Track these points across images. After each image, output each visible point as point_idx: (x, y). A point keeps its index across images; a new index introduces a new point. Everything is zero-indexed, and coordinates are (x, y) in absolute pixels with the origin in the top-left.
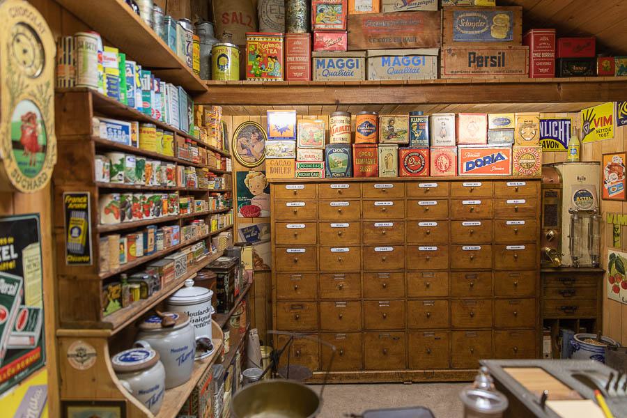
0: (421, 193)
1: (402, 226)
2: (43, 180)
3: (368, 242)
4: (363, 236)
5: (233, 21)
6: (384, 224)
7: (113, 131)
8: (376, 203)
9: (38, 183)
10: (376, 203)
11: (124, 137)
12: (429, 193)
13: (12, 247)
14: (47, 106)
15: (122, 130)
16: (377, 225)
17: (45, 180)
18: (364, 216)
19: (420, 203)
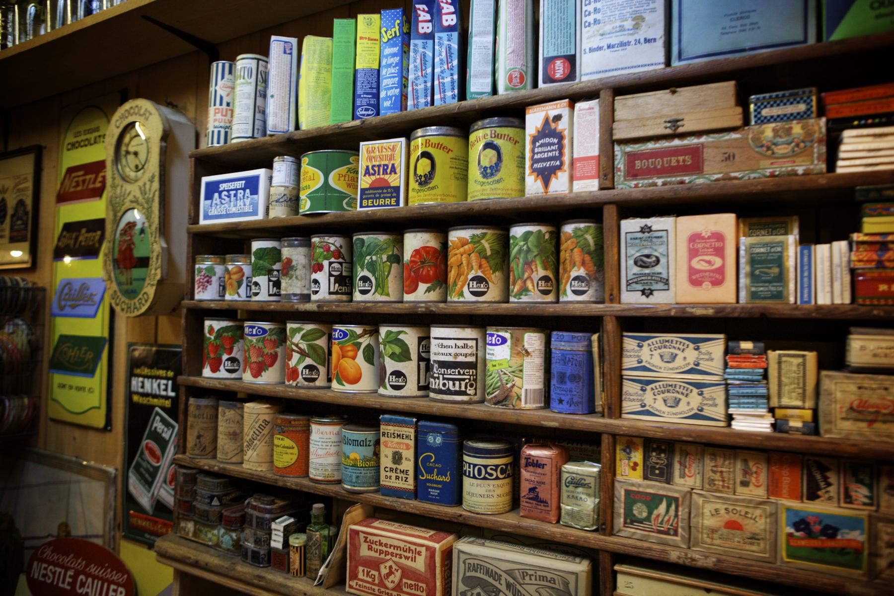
2: (143, 302)
7: (229, 196)
9: (138, 306)
11: (248, 201)
13: (170, 382)
14: (151, 207)
15: (244, 189)
17: (146, 301)
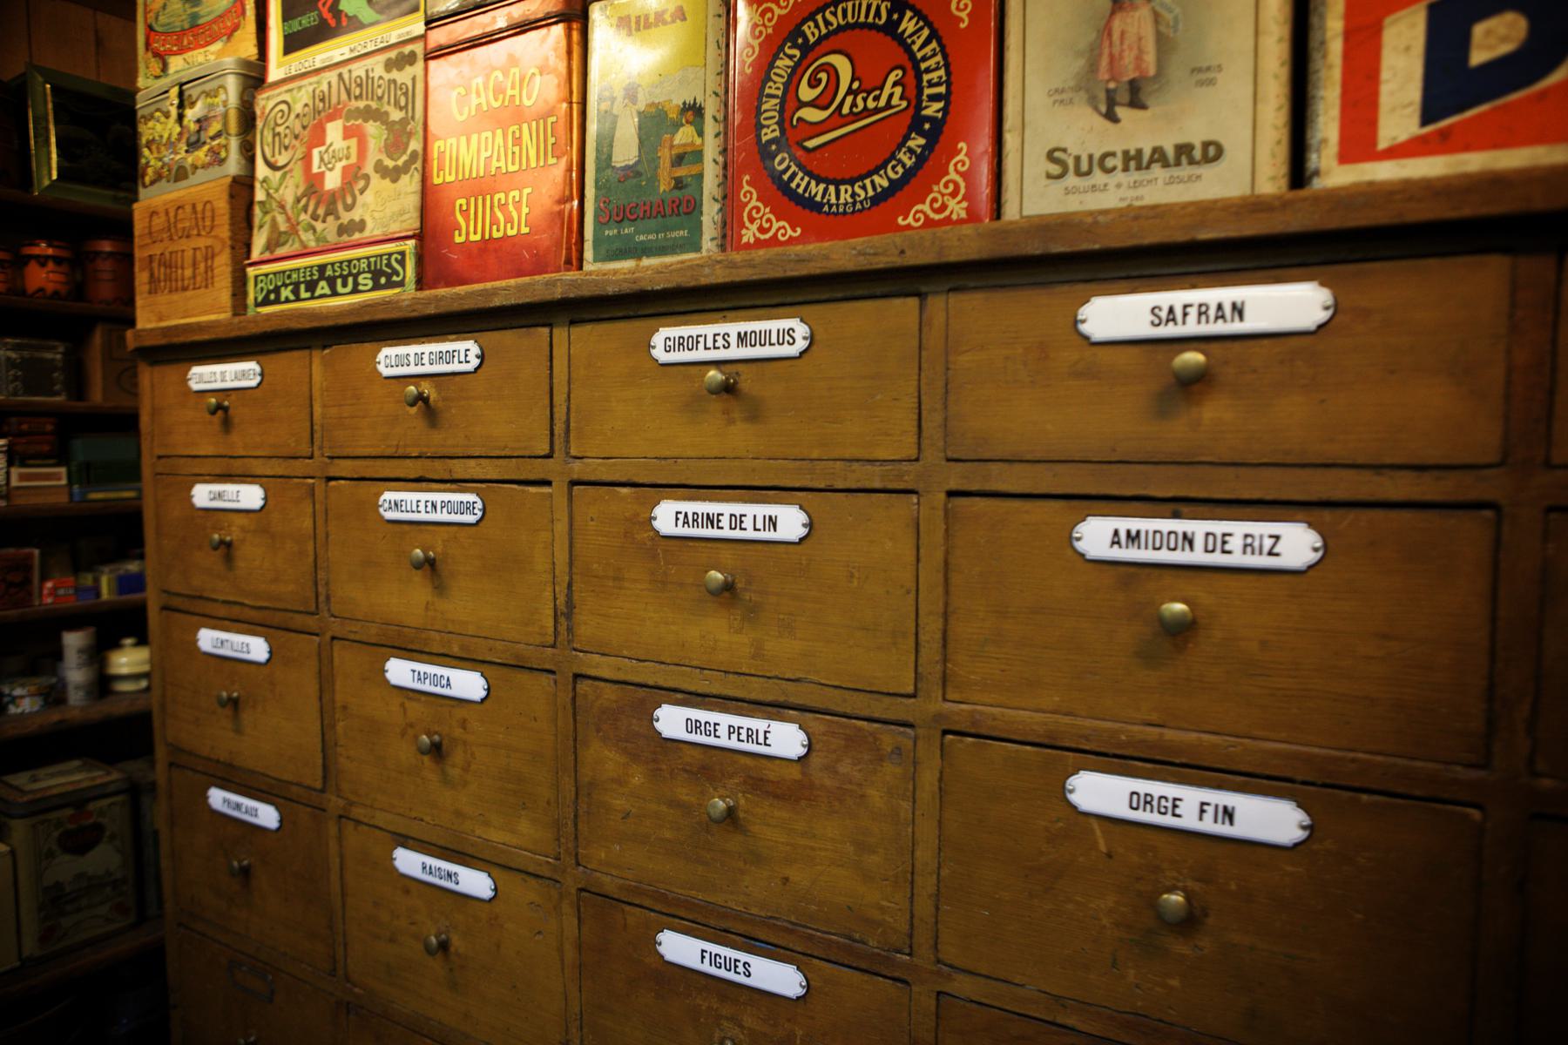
0: (1116, 421)
1: (891, 770)
3: (615, 861)
4: (576, 813)
5: (1217, 318)
6: (725, 729)
8: (667, 516)
10: (667, 516)
12: (1214, 412)
16: (672, 721)
18: (587, 625)
19: (1096, 536)
